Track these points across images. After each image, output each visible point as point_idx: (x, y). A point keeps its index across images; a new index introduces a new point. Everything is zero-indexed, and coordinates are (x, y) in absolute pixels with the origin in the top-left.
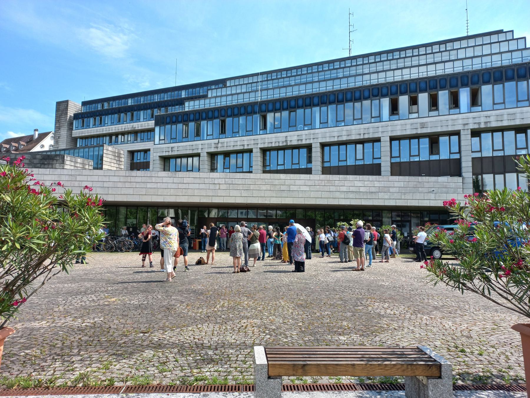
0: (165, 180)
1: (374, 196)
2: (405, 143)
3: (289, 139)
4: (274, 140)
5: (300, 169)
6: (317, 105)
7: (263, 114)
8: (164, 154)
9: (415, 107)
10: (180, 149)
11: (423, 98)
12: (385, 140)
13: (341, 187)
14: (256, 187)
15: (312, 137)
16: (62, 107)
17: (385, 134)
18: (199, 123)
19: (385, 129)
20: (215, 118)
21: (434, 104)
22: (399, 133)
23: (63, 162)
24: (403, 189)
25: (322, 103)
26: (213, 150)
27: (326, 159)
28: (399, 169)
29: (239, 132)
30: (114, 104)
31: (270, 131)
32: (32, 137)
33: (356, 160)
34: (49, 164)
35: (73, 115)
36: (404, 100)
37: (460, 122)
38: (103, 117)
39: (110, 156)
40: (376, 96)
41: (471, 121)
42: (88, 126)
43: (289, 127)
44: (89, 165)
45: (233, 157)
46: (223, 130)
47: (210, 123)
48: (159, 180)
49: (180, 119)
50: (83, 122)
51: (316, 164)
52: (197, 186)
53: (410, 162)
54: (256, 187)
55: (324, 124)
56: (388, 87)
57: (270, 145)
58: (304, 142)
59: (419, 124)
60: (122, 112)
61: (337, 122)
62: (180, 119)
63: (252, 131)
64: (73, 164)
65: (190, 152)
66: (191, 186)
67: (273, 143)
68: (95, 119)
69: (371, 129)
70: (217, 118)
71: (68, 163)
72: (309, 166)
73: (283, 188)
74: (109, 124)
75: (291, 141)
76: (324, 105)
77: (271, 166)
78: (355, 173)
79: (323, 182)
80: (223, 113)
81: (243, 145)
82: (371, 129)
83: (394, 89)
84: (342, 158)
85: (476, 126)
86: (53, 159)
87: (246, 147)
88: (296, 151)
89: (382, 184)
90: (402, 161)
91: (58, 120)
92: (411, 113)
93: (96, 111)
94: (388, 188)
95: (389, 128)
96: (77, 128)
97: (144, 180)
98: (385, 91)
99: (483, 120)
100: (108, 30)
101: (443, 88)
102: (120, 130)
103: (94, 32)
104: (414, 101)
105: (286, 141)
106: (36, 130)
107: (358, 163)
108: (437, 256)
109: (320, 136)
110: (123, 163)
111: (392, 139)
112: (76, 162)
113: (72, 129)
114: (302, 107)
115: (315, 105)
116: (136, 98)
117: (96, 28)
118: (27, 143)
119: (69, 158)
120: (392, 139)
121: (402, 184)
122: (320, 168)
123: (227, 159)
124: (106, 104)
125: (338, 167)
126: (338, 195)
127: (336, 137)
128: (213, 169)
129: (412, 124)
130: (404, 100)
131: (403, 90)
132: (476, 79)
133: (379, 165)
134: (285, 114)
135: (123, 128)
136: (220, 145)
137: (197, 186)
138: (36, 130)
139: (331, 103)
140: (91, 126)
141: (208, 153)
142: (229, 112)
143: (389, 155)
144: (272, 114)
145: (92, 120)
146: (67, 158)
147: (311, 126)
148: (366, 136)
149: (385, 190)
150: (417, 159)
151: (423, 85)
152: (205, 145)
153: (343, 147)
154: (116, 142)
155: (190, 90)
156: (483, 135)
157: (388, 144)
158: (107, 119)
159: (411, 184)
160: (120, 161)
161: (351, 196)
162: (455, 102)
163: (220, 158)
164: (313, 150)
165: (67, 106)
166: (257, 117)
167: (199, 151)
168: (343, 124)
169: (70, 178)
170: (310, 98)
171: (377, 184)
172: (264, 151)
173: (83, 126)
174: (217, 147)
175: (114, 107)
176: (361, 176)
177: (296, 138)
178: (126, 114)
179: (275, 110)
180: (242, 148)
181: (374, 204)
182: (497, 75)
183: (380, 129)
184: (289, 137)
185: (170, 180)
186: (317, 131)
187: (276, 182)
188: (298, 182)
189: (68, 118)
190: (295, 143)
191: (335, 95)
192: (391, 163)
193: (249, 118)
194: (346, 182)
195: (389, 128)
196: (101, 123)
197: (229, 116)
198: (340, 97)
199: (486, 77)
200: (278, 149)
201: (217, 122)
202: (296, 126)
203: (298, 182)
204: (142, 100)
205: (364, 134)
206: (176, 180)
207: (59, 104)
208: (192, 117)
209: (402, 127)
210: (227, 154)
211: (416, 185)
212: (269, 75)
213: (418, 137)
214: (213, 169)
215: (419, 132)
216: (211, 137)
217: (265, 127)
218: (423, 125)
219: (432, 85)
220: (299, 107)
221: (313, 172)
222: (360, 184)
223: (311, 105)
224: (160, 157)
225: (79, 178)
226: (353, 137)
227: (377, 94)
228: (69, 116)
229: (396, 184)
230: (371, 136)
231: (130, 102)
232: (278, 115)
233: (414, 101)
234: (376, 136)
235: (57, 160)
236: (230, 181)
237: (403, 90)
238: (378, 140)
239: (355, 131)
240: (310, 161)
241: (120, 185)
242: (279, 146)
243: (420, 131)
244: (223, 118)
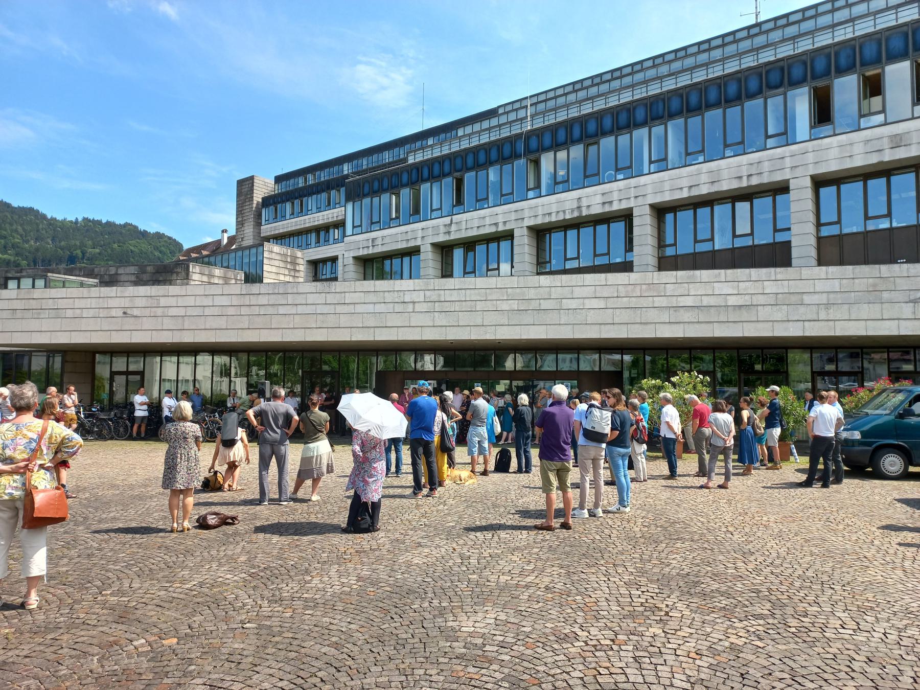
0: (311, 299)
1: (745, 315)
2: (852, 190)
3: (584, 203)
4: (554, 209)
5: (610, 264)
7: (532, 157)
8: (361, 253)
9: (876, 101)
10: (386, 241)
13: (680, 299)
14: (489, 306)
15: (633, 193)
16: (245, 189)
17: (799, 172)
18: (417, 188)
20: (445, 175)
23: (187, 277)
24: (839, 295)
25: (652, 119)
26: (441, 238)
28: (835, 250)
29: (487, 198)
30: (322, 175)
31: (547, 190)
32: (219, 242)
35: (260, 200)
38: (305, 199)
39: (277, 263)
40: (777, 87)
42: (284, 218)
43: (586, 177)
44: (236, 279)
45: (480, 249)
48: (300, 299)
49: (385, 185)
50: (276, 210)
52: (370, 308)
53: (866, 233)
54: (489, 306)
56: (805, 63)
57: (547, 220)
58: (616, 207)
59: (886, 140)
60: (333, 189)
61: (689, 156)
62: (385, 185)
63: (512, 193)
64: (205, 279)
66: (360, 309)
67: (554, 215)
68: (293, 203)
69: (766, 164)
70: (448, 175)
71: (195, 277)
73: (545, 305)
74: (314, 210)
75: (589, 206)
76: (657, 122)
77: (553, 262)
79: (638, 287)
80: (459, 162)
81: (496, 224)
82: (766, 164)
83: (820, 65)
84: (703, 234)
86: (172, 272)
87: (501, 228)
88: (602, 229)
89: (784, 287)
90: (846, 231)
91: (240, 212)
92: (864, 116)
93: (296, 189)
94: (800, 296)
95: (811, 158)
96: (268, 222)
98: (797, 72)
100: (383, 64)
102: (330, 220)
103: (363, 70)
105: (579, 207)
106: (224, 231)
107: (739, 243)
108: (892, 469)
109: (649, 190)
110: (302, 274)
111: (819, 182)
112: (211, 276)
113: (260, 224)
114: (611, 132)
115: (638, 126)
116: (355, 162)
117: (368, 63)
119: (197, 269)
120: (819, 182)
121: (836, 285)
122: (652, 261)
123: (471, 254)
126: (652, 315)
127: (686, 190)
128: (446, 272)
129: (867, 141)
131: (843, 62)
133: (787, 245)
134: (577, 151)
135: (335, 215)
136: (453, 228)
137: (370, 308)
138: (224, 231)
139: (672, 116)
141: (433, 245)
143: (812, 217)
144: (551, 155)
145: (288, 206)
146: (195, 270)
148: (755, 181)
149: (795, 300)
150: (884, 224)
152: (426, 232)
153: (704, 212)
154: (327, 241)
157: (809, 193)
158: (311, 202)
160: (295, 270)
161: (687, 316)
164: (636, 222)
165: (253, 186)
167: (418, 243)
168: (701, 159)
169: (150, 302)
170: (629, 110)
171: (770, 288)
174: (449, 233)
175: (322, 179)
176: (729, 271)
177: (599, 199)
178: (339, 191)
179: (556, 146)
180: (493, 229)
181: (747, 335)
183: (788, 162)
184: (584, 200)
185: (320, 299)
186: (643, 180)
187: (532, 294)
188: (578, 292)
189: (254, 205)
190: (597, 210)
191: (681, 96)
192: (819, 239)
193: (507, 168)
194: (691, 286)
195: (811, 158)
196: (302, 211)
197: (469, 170)
201: (448, 182)
202: (598, 174)
203: (578, 292)
204: (365, 163)
205: (749, 176)
206: (331, 298)
207: (240, 183)
209: (841, 150)
210: (469, 245)
211: (875, 285)
212: (577, 86)
213: (886, 171)
215: (887, 159)
216: (438, 213)
218: (897, 141)
220: (604, 134)
221: (635, 269)
222: (727, 289)
223: (631, 125)
224: (355, 258)
226: (725, 186)
227: (778, 81)
228: (255, 202)
229: (820, 286)
230: (765, 179)
232: (562, 155)
234: (778, 177)
235: (177, 273)
236: (434, 296)
237: (843, 62)
238: (782, 188)
241: (231, 311)
242: (564, 220)
243: (888, 156)
244: (457, 174)
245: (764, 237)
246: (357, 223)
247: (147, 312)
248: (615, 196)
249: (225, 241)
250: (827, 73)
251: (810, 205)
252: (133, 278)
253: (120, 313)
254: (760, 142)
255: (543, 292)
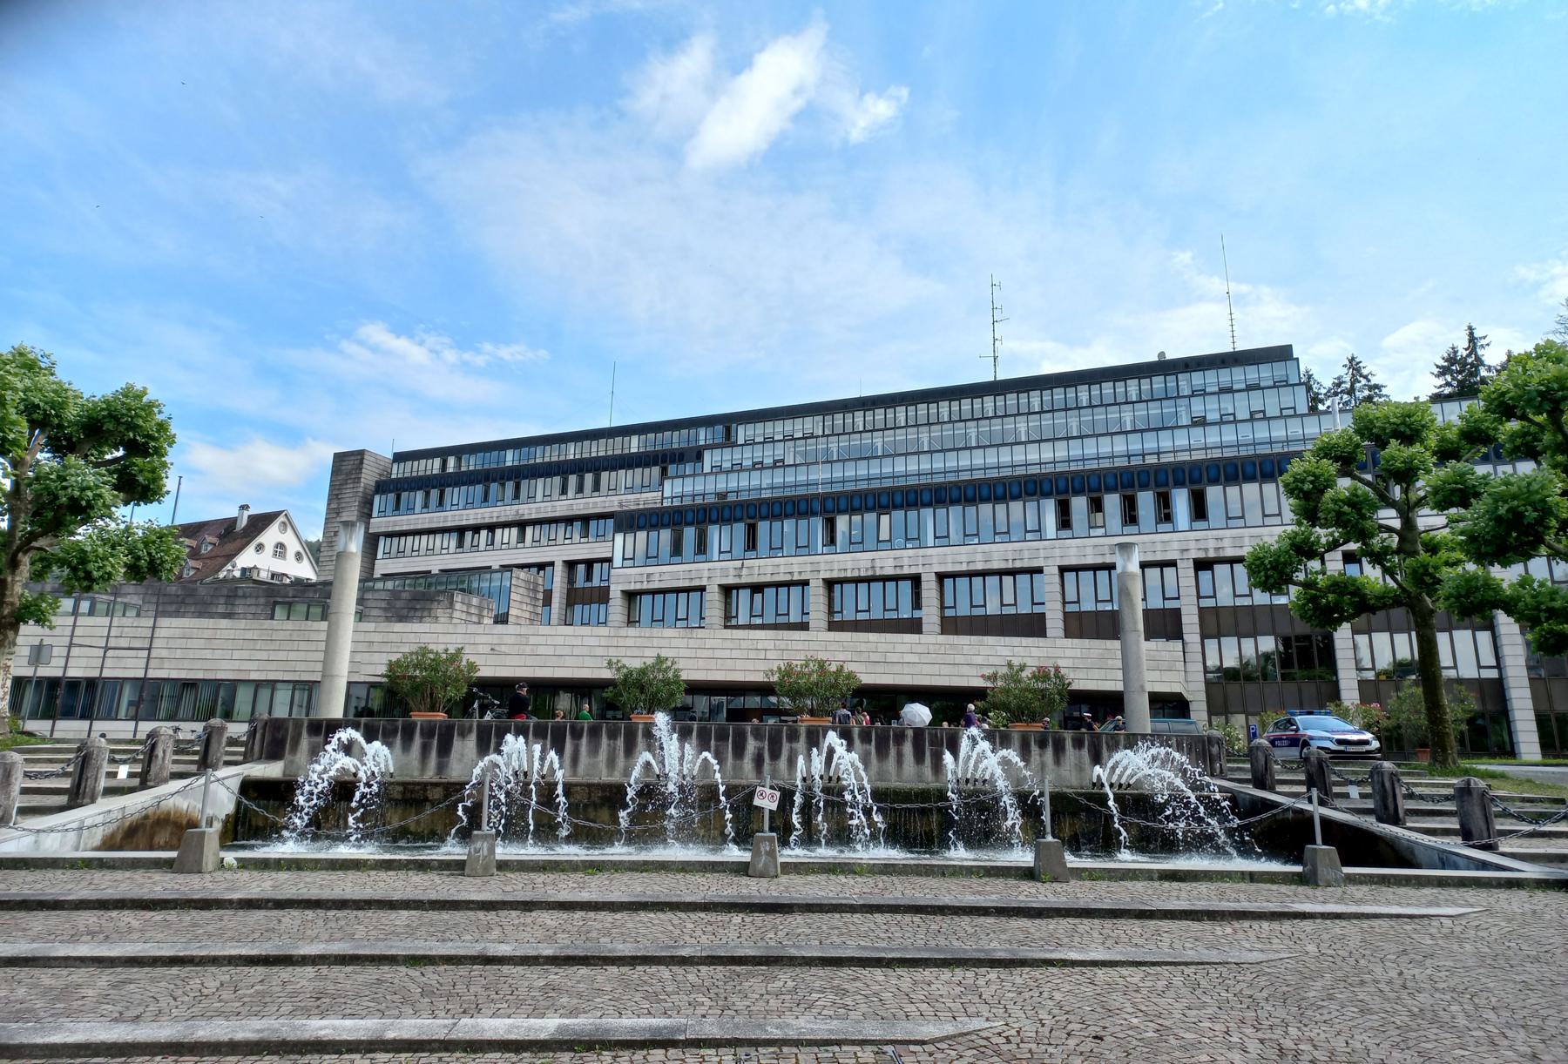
0: (675, 643)
3: (878, 564)
6: (929, 505)
8: (632, 587)
9: (1099, 515)
11: (1112, 502)
12: (1052, 571)
16: (348, 465)
17: (1050, 562)
19: (1048, 553)
21: (1130, 517)
22: (1073, 561)
23: (451, 606)
26: (731, 581)
27: (949, 601)
32: (234, 520)
33: (1002, 605)
34: (423, 609)
36: (1079, 504)
37: (1176, 546)
38: (448, 490)
41: (1192, 545)
42: (411, 510)
45: (770, 592)
46: (751, 544)
47: (726, 529)
51: (930, 614)
55: (942, 539)
58: (906, 571)
65: (687, 584)
68: (428, 494)
71: (458, 606)
72: (917, 614)
73: (874, 657)
78: (1002, 632)
84: (978, 600)
85: (1201, 555)
86: (432, 600)
87: (796, 577)
95: (1057, 552)
96: (383, 513)
97: (639, 642)
99: (1211, 544)
101: (1144, 486)
104: (1097, 506)
106: (244, 507)
107: (1006, 611)
112: (469, 605)
113: (370, 516)
115: (925, 505)
118: (220, 537)
120: (1063, 570)
121: (1078, 653)
122: (937, 620)
124: (451, 461)
125: (971, 617)
130: (1079, 504)
131: (1077, 485)
132: (1196, 474)
136: (745, 572)
137: (727, 654)
140: (418, 508)
142: (764, 511)
143: (1059, 597)
145: (420, 495)
147: (918, 541)
151: (1111, 481)
152: (714, 571)
155: (651, 436)
156: (1217, 567)
157: (1057, 579)
158: (455, 494)
159: (1094, 653)
162: (1165, 515)
163: (744, 595)
166: (818, 523)
167: (704, 583)
172: (830, 584)
173: (397, 507)
177: (891, 562)
178: (503, 485)
179: (851, 510)
182: (1230, 470)
183: (1042, 553)
185: (683, 643)
187: (863, 647)
188: (899, 648)
190: (889, 571)
192: (1065, 613)
195: (1057, 552)
197: (763, 518)
198: (970, 493)
199: (1213, 473)
200: (857, 581)
203: (899, 648)
206: (692, 643)
208: (690, 517)
214: (729, 621)
216: (728, 556)
217: (832, 541)
219: (1125, 479)
225: (532, 640)
226: (996, 565)
229: (1069, 653)
230: (1026, 564)
231: (510, 458)
233: (1097, 506)
234: (1035, 564)
236: (782, 645)
239: (998, 555)
240: (917, 603)
245: (1025, 608)
246: (629, 554)
247: (515, 650)
248: (906, 562)
249: (245, 522)
250: (1067, 492)
251: (1058, 588)
252: (383, 605)
253: (487, 649)
254: (1021, 535)
255: (872, 647)
